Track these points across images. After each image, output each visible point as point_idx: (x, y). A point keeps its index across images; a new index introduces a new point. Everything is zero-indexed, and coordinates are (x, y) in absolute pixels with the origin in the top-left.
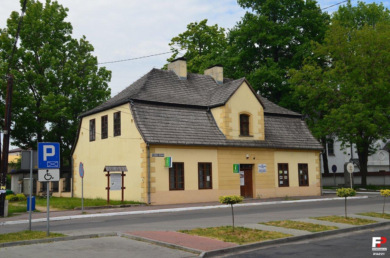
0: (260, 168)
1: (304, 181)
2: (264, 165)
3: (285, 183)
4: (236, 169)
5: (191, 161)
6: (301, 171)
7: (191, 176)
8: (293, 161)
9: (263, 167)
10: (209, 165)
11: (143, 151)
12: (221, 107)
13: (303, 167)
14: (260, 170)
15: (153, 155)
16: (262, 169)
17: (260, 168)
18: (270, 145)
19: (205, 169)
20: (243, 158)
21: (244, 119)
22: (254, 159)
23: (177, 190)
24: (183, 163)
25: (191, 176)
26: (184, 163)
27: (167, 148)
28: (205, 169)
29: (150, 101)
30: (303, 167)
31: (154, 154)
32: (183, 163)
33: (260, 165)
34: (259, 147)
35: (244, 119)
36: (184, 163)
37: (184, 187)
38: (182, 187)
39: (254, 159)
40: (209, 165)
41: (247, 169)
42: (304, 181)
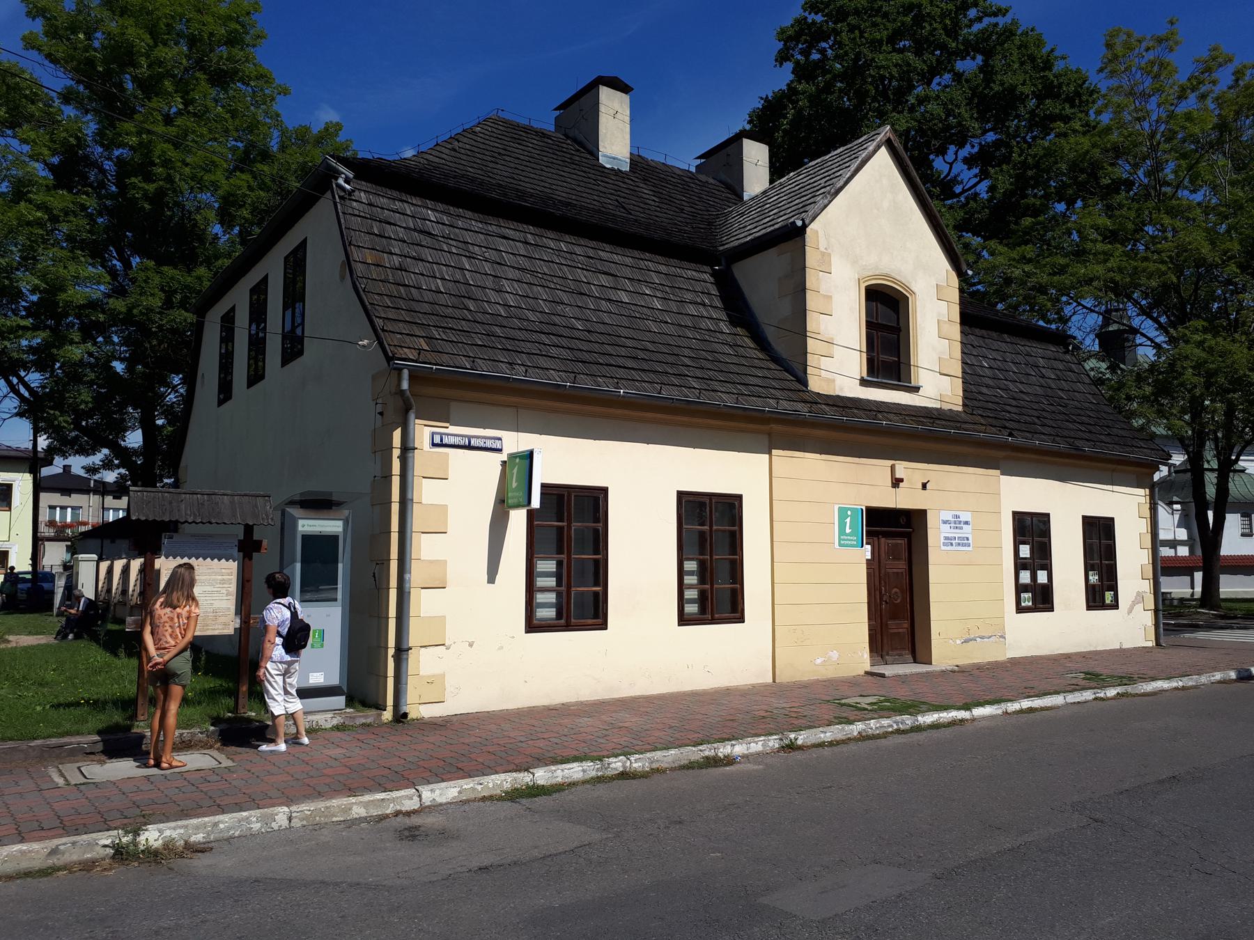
0: (946, 530)
1: (1101, 594)
2: (965, 516)
3: (1042, 599)
4: (848, 531)
5: (642, 483)
6: (340, 523)
7: (642, 554)
8: (1067, 503)
9: (957, 523)
10: (730, 506)
11: (381, 414)
12: (783, 246)
13: (1099, 533)
14: (946, 538)
15: (437, 440)
16: (957, 534)
17: (946, 530)
18: (979, 434)
19: (709, 529)
20: (869, 482)
21: (886, 310)
22: (924, 486)
23: (713, 621)
24: (739, 498)
25: (642, 554)
26: (740, 497)
27: (516, 406)
28: (709, 529)
29: (756, 238)
30: (1099, 533)
31: (441, 434)
32: (739, 498)
33: (947, 515)
34: (926, 437)
35: (886, 310)
36: (740, 497)
37: (743, 610)
38: (596, 616)
39: (924, 486)
40: (730, 506)
41: (896, 537)
42: (1101, 594)
